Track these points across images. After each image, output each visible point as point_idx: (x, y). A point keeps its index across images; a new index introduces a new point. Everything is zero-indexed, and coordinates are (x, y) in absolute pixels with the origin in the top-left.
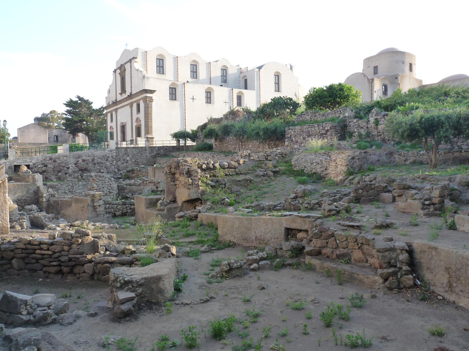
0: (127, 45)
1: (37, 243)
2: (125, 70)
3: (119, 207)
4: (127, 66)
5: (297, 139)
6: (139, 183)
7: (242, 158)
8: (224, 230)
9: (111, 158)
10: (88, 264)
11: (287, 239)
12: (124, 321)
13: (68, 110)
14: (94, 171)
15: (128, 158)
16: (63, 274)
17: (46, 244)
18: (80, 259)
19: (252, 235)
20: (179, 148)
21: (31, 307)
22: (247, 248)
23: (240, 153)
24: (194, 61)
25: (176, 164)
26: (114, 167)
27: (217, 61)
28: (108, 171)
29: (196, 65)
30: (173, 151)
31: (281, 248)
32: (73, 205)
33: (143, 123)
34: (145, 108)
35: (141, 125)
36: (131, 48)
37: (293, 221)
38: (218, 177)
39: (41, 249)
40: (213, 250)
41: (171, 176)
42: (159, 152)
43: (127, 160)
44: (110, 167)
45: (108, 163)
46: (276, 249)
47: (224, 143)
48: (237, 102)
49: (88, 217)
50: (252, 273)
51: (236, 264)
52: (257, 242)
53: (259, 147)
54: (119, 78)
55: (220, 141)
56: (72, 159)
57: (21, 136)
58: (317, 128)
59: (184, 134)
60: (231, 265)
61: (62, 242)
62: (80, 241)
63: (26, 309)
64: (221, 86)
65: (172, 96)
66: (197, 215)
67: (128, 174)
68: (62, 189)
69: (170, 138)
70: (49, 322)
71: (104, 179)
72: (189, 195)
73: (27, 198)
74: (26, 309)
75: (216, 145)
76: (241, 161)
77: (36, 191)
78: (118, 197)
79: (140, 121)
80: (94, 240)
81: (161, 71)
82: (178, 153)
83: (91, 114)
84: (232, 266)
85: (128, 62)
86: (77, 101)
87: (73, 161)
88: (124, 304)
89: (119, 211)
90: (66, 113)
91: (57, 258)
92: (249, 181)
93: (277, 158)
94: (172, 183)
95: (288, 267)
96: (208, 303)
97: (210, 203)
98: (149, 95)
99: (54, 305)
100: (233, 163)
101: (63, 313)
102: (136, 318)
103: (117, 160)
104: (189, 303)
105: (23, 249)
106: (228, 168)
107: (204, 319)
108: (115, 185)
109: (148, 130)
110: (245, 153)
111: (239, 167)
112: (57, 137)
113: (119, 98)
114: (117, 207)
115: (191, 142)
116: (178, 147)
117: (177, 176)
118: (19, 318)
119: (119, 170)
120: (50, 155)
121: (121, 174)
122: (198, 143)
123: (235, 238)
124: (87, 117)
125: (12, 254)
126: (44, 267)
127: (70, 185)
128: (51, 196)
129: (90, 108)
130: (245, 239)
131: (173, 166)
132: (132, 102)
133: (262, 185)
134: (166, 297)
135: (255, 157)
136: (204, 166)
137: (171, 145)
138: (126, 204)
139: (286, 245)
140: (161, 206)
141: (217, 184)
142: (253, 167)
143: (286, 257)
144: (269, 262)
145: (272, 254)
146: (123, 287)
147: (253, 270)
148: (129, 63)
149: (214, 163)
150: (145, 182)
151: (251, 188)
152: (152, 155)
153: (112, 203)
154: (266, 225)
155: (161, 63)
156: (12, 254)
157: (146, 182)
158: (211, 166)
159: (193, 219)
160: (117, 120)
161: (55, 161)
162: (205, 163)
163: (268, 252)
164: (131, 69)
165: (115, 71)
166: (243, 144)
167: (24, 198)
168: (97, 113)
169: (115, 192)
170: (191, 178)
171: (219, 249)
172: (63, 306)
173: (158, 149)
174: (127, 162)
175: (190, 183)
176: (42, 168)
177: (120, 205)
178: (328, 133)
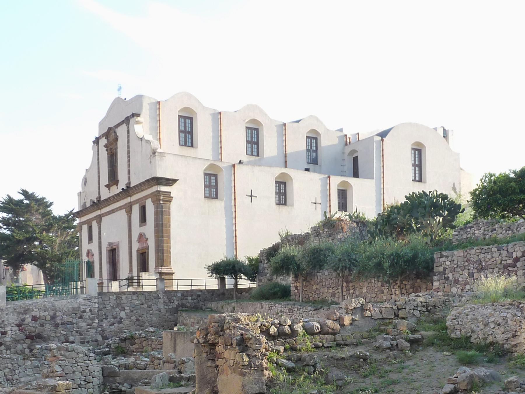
0: (120, 89)
2: (116, 139)
4: (121, 131)
5: (457, 275)
6: (144, 363)
7: (347, 313)
9: (89, 313)
13: (3, 218)
14: (56, 339)
15: (123, 314)
20: (223, 294)
25: (217, 325)
26: (94, 331)
27: (298, 122)
28: (82, 339)
30: (212, 301)
35: (147, 248)
36: (128, 95)
38: (300, 350)
41: (207, 349)
42: (184, 301)
43: (121, 318)
44: (88, 331)
45: (83, 324)
47: (313, 283)
48: (339, 203)
53: (382, 291)
54: (104, 154)
55: (304, 280)
56: (11, 316)
58: (496, 255)
64: (307, 170)
65: (210, 191)
67: (123, 345)
69: (205, 273)
71: (74, 355)
75: (296, 287)
76: (347, 321)
79: (147, 240)
82: (221, 303)
83: (48, 226)
85: (123, 122)
87: (13, 319)
92: (361, 360)
93: (416, 313)
94: (209, 363)
103: (100, 318)
106: (320, 333)
108: (96, 368)
110: (355, 303)
111: (342, 332)
113: (105, 194)
116: (222, 291)
117: (219, 349)
119: (104, 338)
121: (108, 345)
122: (261, 284)
127: (7, 367)
129: (46, 214)
131: (211, 330)
132: (130, 203)
133: (387, 368)
135: (373, 311)
136: (273, 330)
142: (369, 332)
148: (125, 125)
149: (293, 323)
151: (367, 373)
152: (170, 307)
155: (314, 145)
157: (158, 361)
158: (287, 329)
160: (100, 238)
164: (128, 137)
165: (97, 141)
168: (60, 223)
169: (96, 381)
173: (182, 295)
174: (120, 322)
175: (246, 363)
178: (519, 264)
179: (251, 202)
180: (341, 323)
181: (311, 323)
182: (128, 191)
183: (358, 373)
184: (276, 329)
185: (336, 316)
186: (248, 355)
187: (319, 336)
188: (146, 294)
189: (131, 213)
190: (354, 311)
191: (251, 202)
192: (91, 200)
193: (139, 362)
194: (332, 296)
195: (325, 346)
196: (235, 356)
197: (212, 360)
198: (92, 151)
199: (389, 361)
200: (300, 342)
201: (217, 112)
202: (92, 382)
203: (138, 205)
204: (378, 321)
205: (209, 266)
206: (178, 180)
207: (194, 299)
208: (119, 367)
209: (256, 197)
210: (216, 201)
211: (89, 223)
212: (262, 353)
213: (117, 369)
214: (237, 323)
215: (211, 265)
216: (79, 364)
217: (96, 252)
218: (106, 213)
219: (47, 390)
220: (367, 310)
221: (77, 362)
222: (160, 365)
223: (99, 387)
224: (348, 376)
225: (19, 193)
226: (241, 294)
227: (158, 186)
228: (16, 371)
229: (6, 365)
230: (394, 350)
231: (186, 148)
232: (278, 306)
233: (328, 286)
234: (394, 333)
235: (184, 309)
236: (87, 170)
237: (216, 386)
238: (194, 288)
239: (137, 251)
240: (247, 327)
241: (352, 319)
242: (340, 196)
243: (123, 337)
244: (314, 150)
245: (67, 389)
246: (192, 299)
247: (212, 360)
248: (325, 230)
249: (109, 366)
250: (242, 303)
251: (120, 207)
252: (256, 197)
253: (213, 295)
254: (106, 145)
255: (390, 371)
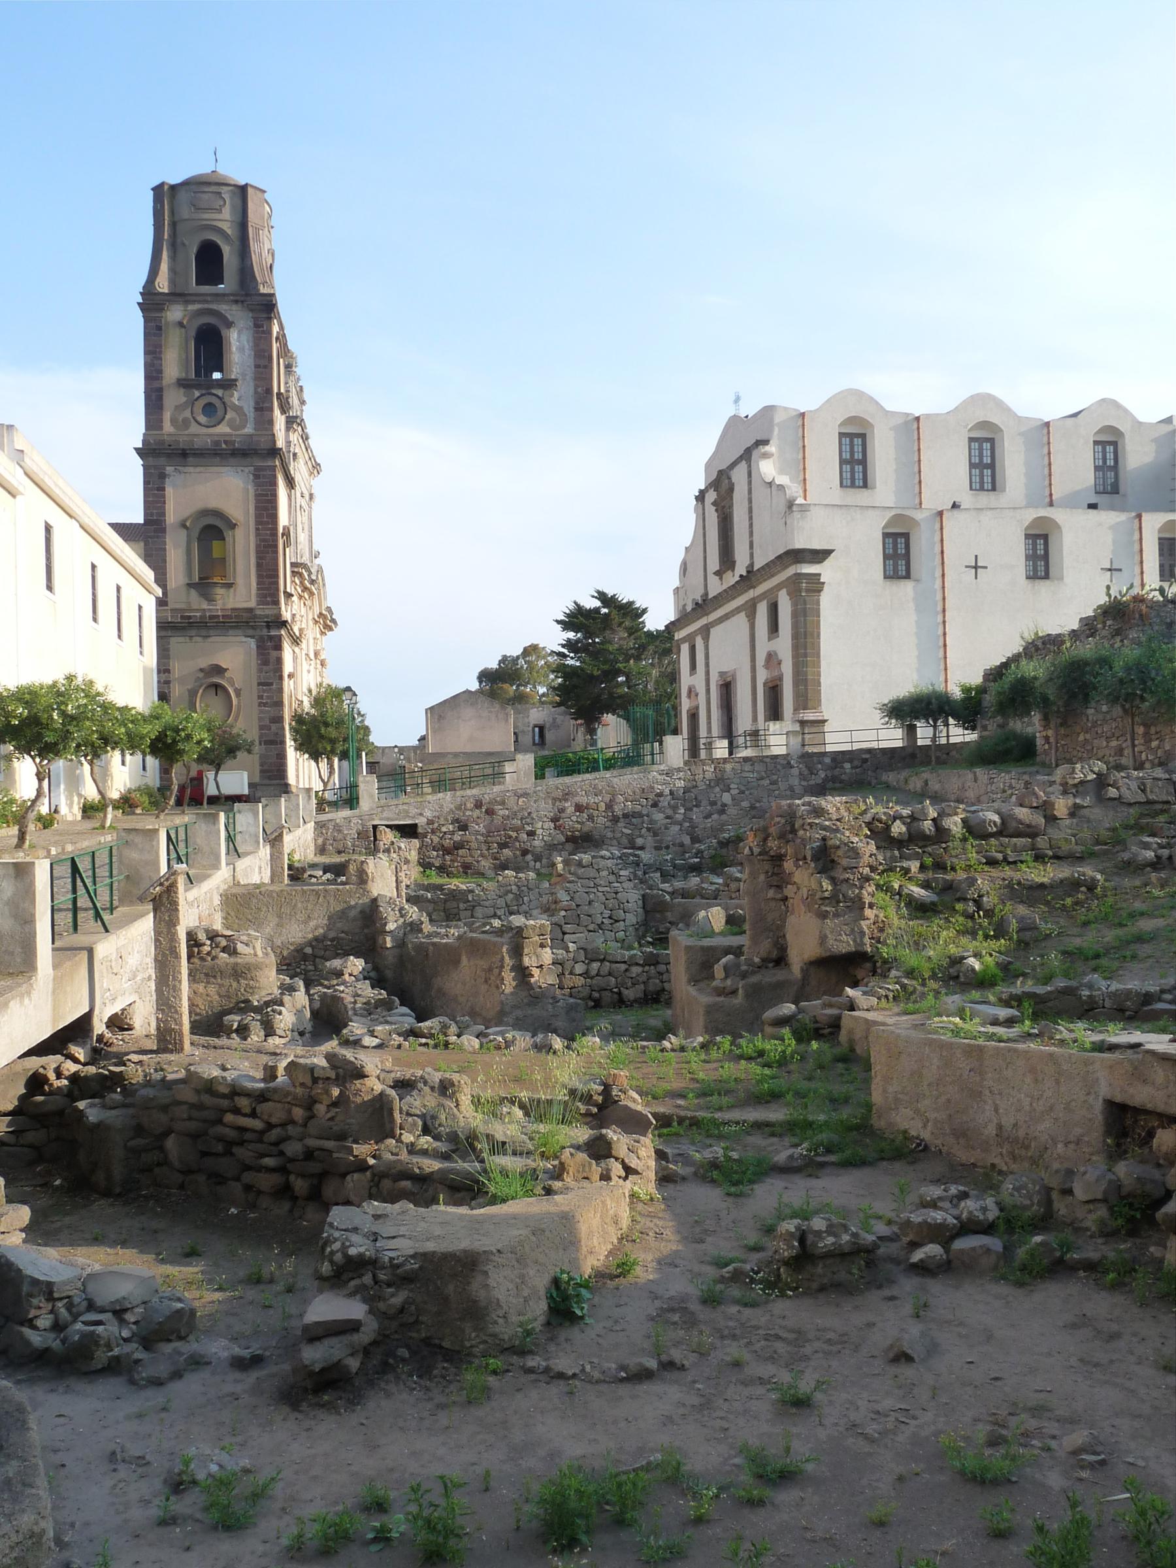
0: (737, 400)
1: (226, 1091)
2: (731, 489)
3: (636, 970)
4: (739, 476)
6: (713, 887)
7: (1065, 792)
8: (891, 1089)
10: (356, 1176)
11: (1116, 1153)
12: (310, 1405)
13: (569, 640)
14: (615, 842)
15: (726, 798)
16: (294, 1199)
17: (247, 1094)
18: (335, 1155)
19: (985, 1119)
20: (913, 756)
21: (70, 1307)
22: (957, 1171)
23: (1059, 773)
24: (984, 425)
25: (783, 821)
26: (677, 828)
27: (1075, 415)
28: (656, 841)
29: (992, 441)
30: (890, 768)
31: (1067, 1186)
32: (464, 960)
33: (787, 669)
34: (795, 615)
35: (780, 678)
36: (749, 408)
37: (1138, 1074)
38: (953, 869)
39: (237, 1111)
40: (823, 1165)
41: (767, 866)
42: (837, 772)
44: (666, 828)
45: (659, 817)
46: (1048, 1190)
47: (1078, 729)
48: (1161, 566)
49: (502, 1003)
50: (908, 1285)
51: (830, 1240)
52: (1004, 1151)
55: (1062, 725)
56: (542, 804)
57: (434, 731)
59: (929, 703)
60: (810, 1238)
61: (288, 1094)
62: (336, 1092)
63: (51, 1312)
64: (1093, 506)
65: (895, 566)
66: (839, 1018)
67: (724, 851)
68: (487, 903)
69: (877, 719)
70: (100, 1366)
71: (592, 873)
72: (823, 939)
73: (343, 935)
74: (51, 1312)
75: (1047, 738)
76: (1061, 806)
77: (368, 911)
78: (644, 936)
79: (780, 663)
80: (382, 1094)
81: (859, 476)
82: (904, 774)
83: (639, 648)
84: (814, 1244)
85: (741, 458)
86: (597, 610)
87: (545, 809)
88: (318, 1343)
89: (634, 985)
90: (565, 651)
91: (276, 1144)
92: (1083, 889)
94: (771, 893)
95: (1082, 1274)
96: (645, 1387)
97: (898, 974)
98: (808, 569)
99: (140, 1310)
100: (1022, 813)
101: (170, 1341)
102: (355, 1400)
103: (688, 805)
104: (570, 1373)
105: (193, 1106)
106: (1000, 833)
107: (574, 1450)
108: (632, 896)
109: (807, 694)
110: (1083, 772)
111: (1049, 831)
112: (542, 729)
113: (716, 587)
114: (626, 970)
115: (960, 731)
116: (910, 750)
117: (788, 865)
118: (21, 1334)
119: (695, 840)
120: (475, 791)
121: (699, 853)
122: (985, 733)
123: (925, 1126)
124: (628, 661)
125: (164, 1118)
126: (244, 1171)
127: (510, 891)
128: (412, 930)
129: (636, 629)
130: (962, 1134)
131: (772, 830)
133: (1138, 905)
134: (494, 1335)
135: (1127, 785)
136: (898, 829)
137: (883, 745)
138: (658, 963)
139: (1088, 1176)
140: (726, 977)
141: (947, 898)
142: (1114, 830)
143: (1087, 1229)
144: (995, 1243)
145: (1025, 1208)
146: (345, 1277)
147: (923, 1269)
148: (744, 462)
149: (942, 814)
150: (733, 886)
151: (1091, 916)
152: (811, 782)
153: (610, 958)
154: (1036, 1081)
155: (858, 449)
156: (164, 1118)
158: (928, 826)
159: (826, 1031)
160: (707, 665)
161: (490, 812)
162: (901, 818)
163: (1008, 1201)
164: (750, 483)
165: (701, 497)
166: (1153, 730)
167: (332, 935)
168: (657, 643)
169: (631, 919)
170: (833, 874)
171: (848, 1164)
172: (169, 1318)
173: (834, 760)
174: (722, 812)
175: (826, 894)
176: (453, 833)
177: (637, 964)
179: (976, 578)
180: (1048, 812)
181: (981, 814)
182: (750, 578)
183: (1072, 917)
184: (904, 829)
185: (1037, 798)
186: (833, 880)
187: (998, 840)
188: (768, 760)
189: (754, 618)
190: (1081, 789)
191: (976, 578)
192: (694, 599)
193: (705, 885)
194: (1115, 754)
195: (1010, 860)
196: (810, 880)
197: (777, 886)
198: (695, 515)
199: (1147, 892)
200: (954, 853)
201: (910, 418)
202: (624, 921)
203: (765, 602)
204: (1137, 808)
205: (884, 705)
206: (833, 551)
207: (857, 767)
208: (672, 894)
209: (986, 567)
210: (1047, 582)
211: (690, 639)
212: (861, 874)
213: (667, 897)
214: (819, 817)
215: (886, 702)
216: (600, 889)
217: (701, 689)
218: (715, 620)
219: (510, 935)
220: (1109, 785)
221: (596, 886)
222: (739, 891)
223: (637, 930)
224: (1046, 922)
225: (593, 597)
226: (948, 754)
227: (798, 565)
228: (525, 898)
229: (509, 888)
230: (1163, 868)
231: (853, 490)
232: (1007, 778)
233: (1109, 734)
234: (1167, 833)
235: (837, 785)
236: (686, 548)
237: (784, 936)
238: (856, 747)
239: (765, 684)
240: (838, 823)
241: (1075, 804)
242: (1165, 550)
243: (724, 838)
244: (1110, 466)
245: (543, 935)
246: (852, 768)
247: (777, 886)
248: (1109, 623)
249: (655, 892)
250: (940, 771)
251: (738, 608)
252: (986, 567)
253: (892, 758)
254: (715, 501)
255: (1142, 914)
